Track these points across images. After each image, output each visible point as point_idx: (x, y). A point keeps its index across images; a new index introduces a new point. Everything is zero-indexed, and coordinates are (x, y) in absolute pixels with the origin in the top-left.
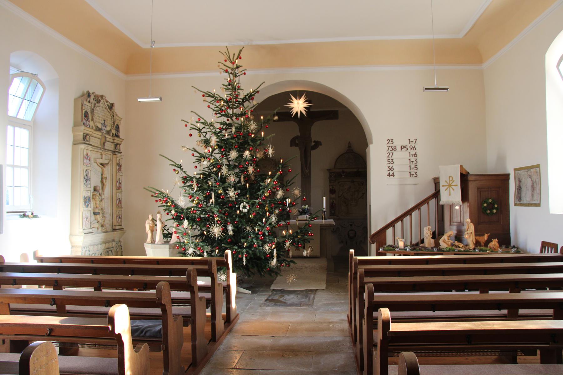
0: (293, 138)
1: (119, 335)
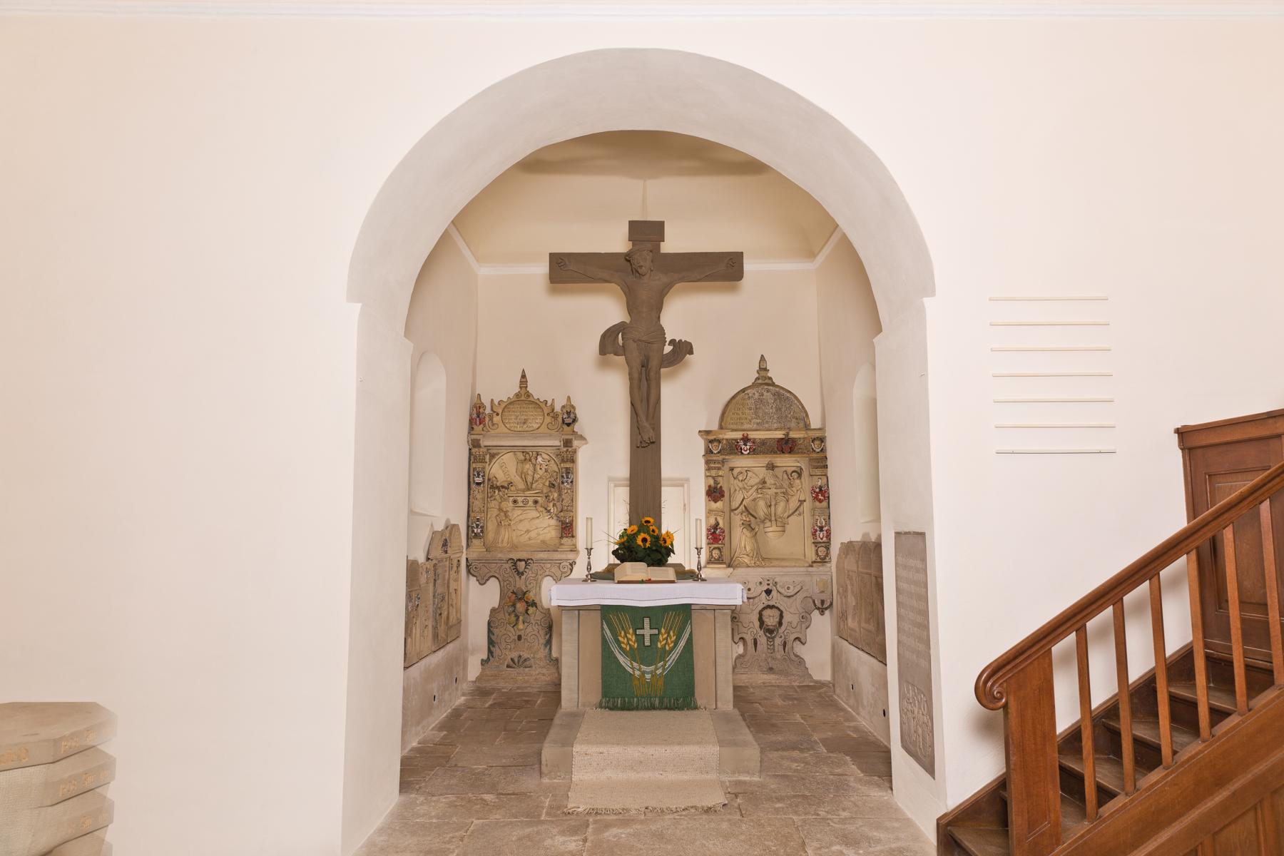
0: (604, 337)
1: (441, 727)
